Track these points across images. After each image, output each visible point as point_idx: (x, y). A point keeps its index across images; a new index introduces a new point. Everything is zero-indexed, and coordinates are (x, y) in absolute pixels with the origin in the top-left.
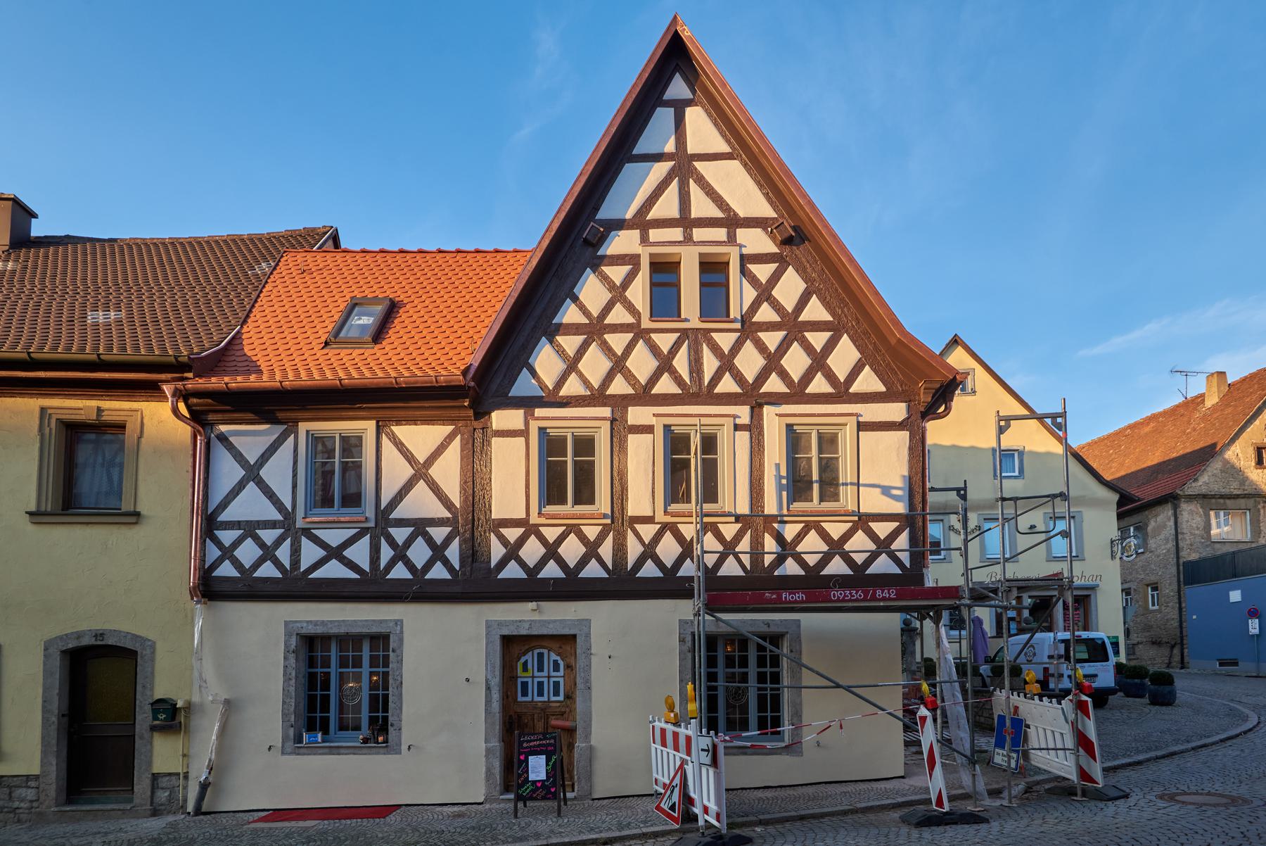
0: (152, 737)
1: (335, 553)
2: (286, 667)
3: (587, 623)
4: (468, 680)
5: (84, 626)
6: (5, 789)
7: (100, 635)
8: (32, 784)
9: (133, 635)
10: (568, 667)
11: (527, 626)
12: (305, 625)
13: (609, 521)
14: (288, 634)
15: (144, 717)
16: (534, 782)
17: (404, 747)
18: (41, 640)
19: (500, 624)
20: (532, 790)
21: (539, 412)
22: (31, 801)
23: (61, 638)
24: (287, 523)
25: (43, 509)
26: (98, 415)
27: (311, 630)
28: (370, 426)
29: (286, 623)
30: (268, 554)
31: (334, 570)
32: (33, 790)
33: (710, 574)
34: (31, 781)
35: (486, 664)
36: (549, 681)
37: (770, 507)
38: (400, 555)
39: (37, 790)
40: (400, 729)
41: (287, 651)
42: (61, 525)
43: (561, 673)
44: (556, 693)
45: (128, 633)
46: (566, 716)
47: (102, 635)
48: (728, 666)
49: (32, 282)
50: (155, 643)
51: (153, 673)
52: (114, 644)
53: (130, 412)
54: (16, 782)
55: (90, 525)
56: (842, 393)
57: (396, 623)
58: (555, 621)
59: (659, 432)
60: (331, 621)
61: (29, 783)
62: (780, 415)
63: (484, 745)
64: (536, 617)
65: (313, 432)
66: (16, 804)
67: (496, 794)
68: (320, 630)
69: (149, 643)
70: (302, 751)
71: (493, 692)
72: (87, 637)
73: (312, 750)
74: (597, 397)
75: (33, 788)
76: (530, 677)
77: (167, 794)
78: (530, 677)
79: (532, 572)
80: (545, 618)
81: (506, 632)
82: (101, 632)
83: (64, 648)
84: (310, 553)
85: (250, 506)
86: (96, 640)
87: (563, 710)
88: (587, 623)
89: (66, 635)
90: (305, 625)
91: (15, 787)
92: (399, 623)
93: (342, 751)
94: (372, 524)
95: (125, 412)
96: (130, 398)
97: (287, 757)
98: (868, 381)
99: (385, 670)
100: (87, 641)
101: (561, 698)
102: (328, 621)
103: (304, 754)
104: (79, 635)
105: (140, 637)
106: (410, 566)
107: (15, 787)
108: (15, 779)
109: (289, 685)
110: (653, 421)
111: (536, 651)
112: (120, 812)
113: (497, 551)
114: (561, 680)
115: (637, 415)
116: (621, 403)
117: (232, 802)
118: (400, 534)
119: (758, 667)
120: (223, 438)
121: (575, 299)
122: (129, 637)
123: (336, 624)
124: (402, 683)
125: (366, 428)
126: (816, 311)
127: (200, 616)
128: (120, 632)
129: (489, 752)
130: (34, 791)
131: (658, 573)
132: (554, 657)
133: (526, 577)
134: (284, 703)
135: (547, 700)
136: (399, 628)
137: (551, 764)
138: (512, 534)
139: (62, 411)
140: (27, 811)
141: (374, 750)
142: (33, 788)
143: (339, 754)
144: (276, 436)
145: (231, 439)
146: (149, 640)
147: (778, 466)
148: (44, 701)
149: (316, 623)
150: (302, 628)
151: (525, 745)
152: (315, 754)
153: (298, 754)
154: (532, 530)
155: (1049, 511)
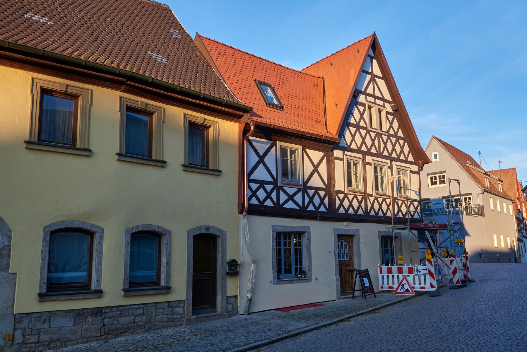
0: (226, 279)
1: (291, 198)
2: (273, 245)
3: (358, 230)
4: (330, 251)
5: (201, 224)
6: (170, 309)
7: (208, 228)
8: (181, 305)
9: (219, 229)
10: (350, 247)
11: (344, 231)
12: (279, 227)
13: (363, 195)
14: (273, 231)
15: (221, 268)
16: (367, 287)
17: (313, 279)
18: (186, 230)
19: (337, 230)
20: (367, 290)
21: (347, 153)
22: (181, 314)
23: (193, 229)
24: (274, 183)
25: (33, 140)
26: (204, 122)
27: (281, 229)
28: (300, 147)
29: (273, 226)
30: (269, 196)
31: (290, 205)
32: (182, 308)
33: (395, 215)
34: (181, 303)
35: (334, 245)
36: (345, 253)
37: (395, 196)
38: (311, 201)
39: (183, 308)
40: (311, 272)
41: (273, 239)
42: (209, 175)
43: (347, 250)
44: (347, 258)
45: (217, 228)
46: (350, 266)
47: (208, 228)
48: (285, 245)
49: (86, 14)
50: (226, 233)
51: (226, 248)
52: (213, 233)
53: (214, 123)
54: (175, 304)
55: (204, 174)
56: (406, 161)
57: (308, 228)
58: (351, 230)
59: (373, 165)
60: (288, 226)
61: (180, 305)
62: (397, 165)
63: (335, 277)
64: (346, 228)
65: (282, 146)
66: (175, 316)
67: (340, 296)
68: (284, 230)
69: (225, 233)
70: (280, 282)
71: (337, 256)
72: (203, 229)
73: (284, 282)
74: (359, 151)
75: (182, 307)
76: (344, 250)
77: (231, 306)
78: (344, 250)
79: (347, 210)
80: (348, 228)
81: (339, 233)
82: (208, 227)
83: (195, 234)
84: (283, 197)
85: (260, 174)
86: (206, 231)
87: (349, 263)
88: (358, 230)
89: (195, 228)
90: (279, 227)
91: (174, 307)
92: (309, 228)
93: (294, 282)
94: (302, 187)
95: (213, 122)
96: (216, 117)
97: (275, 285)
98: (411, 158)
99: (296, 247)
100: (203, 231)
101: (348, 259)
102: (286, 226)
103: (281, 284)
104: (200, 228)
105: (222, 230)
106: (314, 205)
107: (174, 307)
108: (174, 303)
109: (274, 254)
110: (372, 162)
111: (341, 241)
112: (218, 316)
113: (338, 203)
114: (348, 252)
115: (369, 159)
116: (364, 154)
117: (258, 307)
118: (254, 186)
119: (295, 256)
120: (250, 142)
121: (353, 115)
122: (218, 230)
123: (289, 227)
124: (311, 252)
125: (299, 148)
126: (400, 134)
127: (243, 220)
128: (215, 227)
129: (337, 279)
130: (181, 309)
131: (313, 209)
132: (346, 243)
133: (375, 215)
134: (273, 261)
135: (344, 260)
136: (309, 230)
137: (369, 280)
138: (341, 196)
139: (129, 101)
140: (179, 320)
141: (303, 281)
142: (182, 307)
143: (292, 283)
144: (269, 145)
145: (253, 143)
146: (224, 232)
147: (396, 181)
148: (188, 261)
149: (282, 227)
150: (278, 228)
151: (361, 274)
152: (284, 284)
153: (279, 284)
154: (346, 196)
155: (83, 146)
